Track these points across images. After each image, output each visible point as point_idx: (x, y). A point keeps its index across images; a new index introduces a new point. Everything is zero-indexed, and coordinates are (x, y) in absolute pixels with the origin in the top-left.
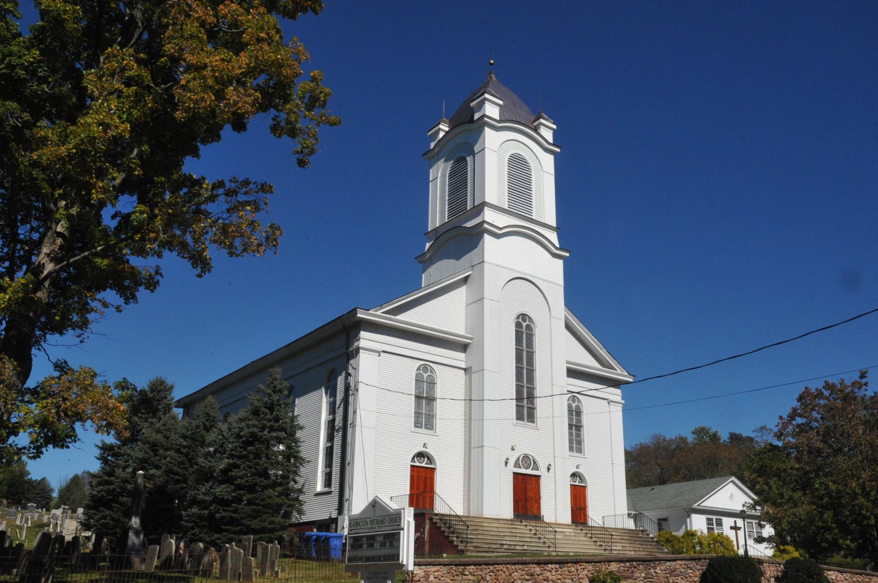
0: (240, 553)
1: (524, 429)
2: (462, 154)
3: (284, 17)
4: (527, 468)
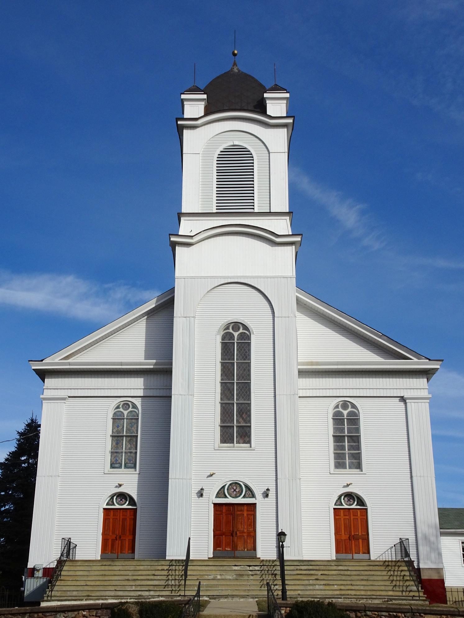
1: (236, 453)
2: (252, 65)
3: (21, 434)
4: (236, 497)
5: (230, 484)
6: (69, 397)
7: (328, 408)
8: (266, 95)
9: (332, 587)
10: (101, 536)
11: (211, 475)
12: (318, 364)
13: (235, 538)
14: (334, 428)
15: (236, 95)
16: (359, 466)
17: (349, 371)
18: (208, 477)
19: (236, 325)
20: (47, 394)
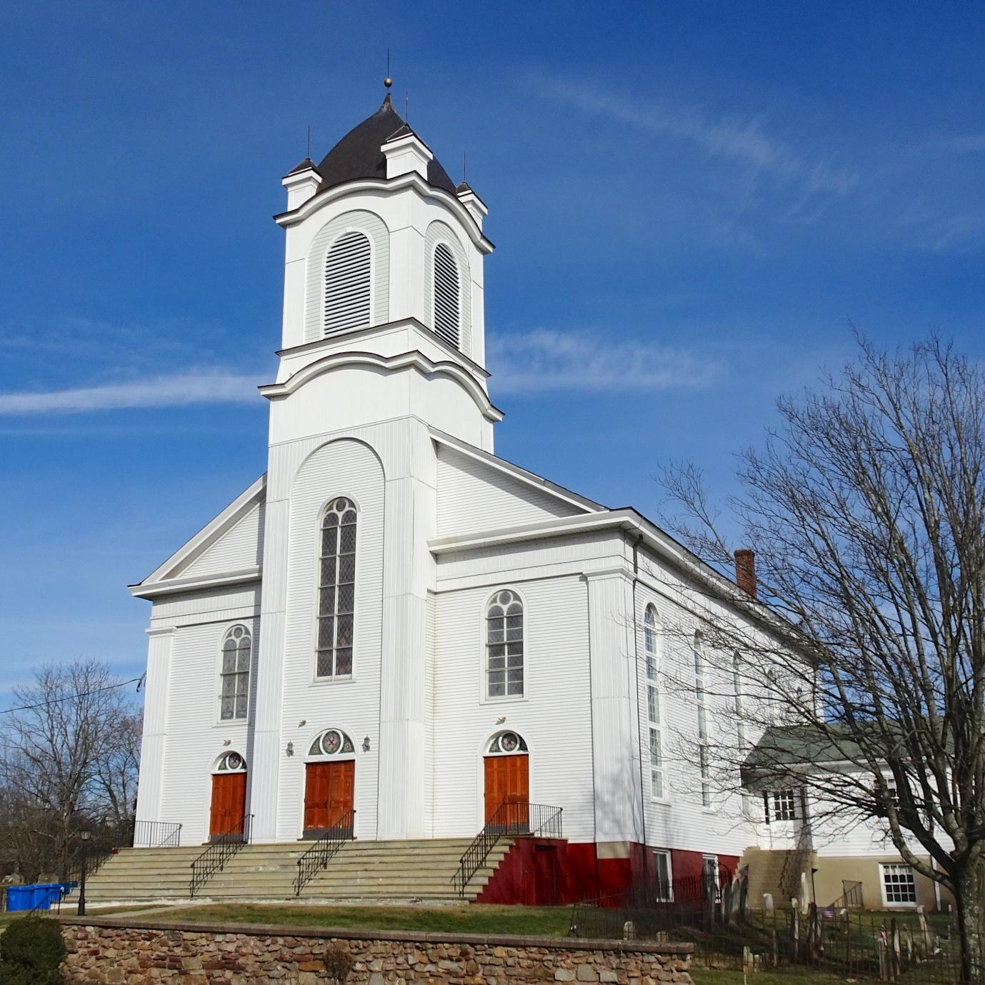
0: (685, 976)
1: (335, 687)
4: (332, 752)
5: (327, 735)
6: (178, 627)
7: (481, 605)
8: (383, 148)
9: (377, 882)
10: (210, 812)
11: (304, 723)
12: (456, 540)
13: (330, 811)
14: (490, 634)
15: (354, 163)
16: (519, 689)
17: (517, 542)
18: (300, 726)
19: (341, 502)
20: (155, 625)
